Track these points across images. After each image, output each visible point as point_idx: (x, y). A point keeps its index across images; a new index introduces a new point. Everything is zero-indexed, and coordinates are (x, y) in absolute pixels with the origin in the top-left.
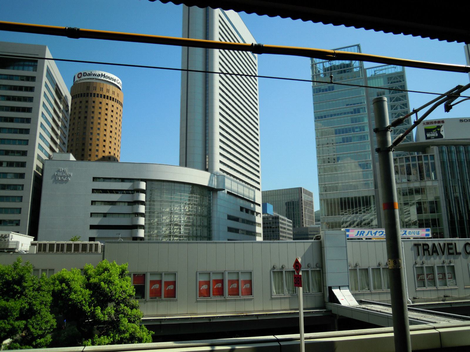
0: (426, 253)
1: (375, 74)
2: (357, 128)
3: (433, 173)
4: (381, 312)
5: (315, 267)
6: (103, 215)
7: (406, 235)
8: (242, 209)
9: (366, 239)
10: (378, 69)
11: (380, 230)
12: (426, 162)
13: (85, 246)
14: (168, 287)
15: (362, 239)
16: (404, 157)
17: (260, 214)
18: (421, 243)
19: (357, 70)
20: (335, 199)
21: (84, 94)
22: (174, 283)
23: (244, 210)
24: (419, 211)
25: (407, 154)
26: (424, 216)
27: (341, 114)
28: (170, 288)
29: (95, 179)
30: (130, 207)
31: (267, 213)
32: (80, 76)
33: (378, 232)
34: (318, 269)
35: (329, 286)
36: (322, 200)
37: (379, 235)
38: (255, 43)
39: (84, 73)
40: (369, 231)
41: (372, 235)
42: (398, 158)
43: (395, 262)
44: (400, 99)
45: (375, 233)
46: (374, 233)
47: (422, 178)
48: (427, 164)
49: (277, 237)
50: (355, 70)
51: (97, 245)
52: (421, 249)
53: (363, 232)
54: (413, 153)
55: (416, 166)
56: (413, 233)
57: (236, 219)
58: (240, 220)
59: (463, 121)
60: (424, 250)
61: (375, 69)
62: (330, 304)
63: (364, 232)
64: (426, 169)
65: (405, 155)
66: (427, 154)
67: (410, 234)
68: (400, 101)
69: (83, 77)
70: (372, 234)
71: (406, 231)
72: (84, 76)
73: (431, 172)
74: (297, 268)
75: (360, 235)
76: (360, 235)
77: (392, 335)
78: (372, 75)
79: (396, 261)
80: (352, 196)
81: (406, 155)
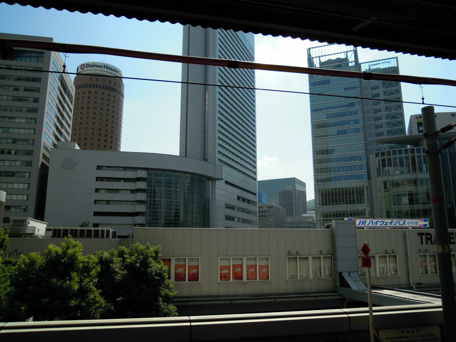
0: (429, 241)
1: (370, 68)
2: (351, 121)
3: (425, 165)
4: (391, 296)
5: (327, 253)
6: (106, 202)
7: (405, 225)
8: (239, 198)
9: (412, 228)
10: (372, 63)
11: (381, 220)
12: (419, 154)
13: (89, 232)
14: (178, 270)
15: (364, 228)
16: (397, 149)
17: (256, 203)
18: (424, 232)
19: (353, 65)
20: (336, 188)
21: (87, 85)
22: (197, 267)
23: (241, 199)
24: (411, 202)
25: (399, 146)
26: (416, 207)
27: (336, 107)
28: (193, 272)
29: (99, 168)
30: (133, 195)
31: (262, 202)
32: (83, 67)
33: (379, 222)
34: (329, 256)
35: (340, 271)
36: (317, 190)
37: (380, 225)
38: (240, 33)
39: (87, 65)
40: (397, 221)
41: (373, 225)
42: (391, 150)
43: (443, 247)
44: (394, 93)
45: (376, 223)
46: (375, 223)
47: (414, 170)
48: (419, 157)
49: (4, 222)
50: (350, 64)
51: (108, 231)
52: (424, 237)
53: (364, 222)
54: (406, 145)
55: (409, 159)
56: (412, 223)
57: (233, 208)
58: (236, 208)
59: (455, 115)
60: (427, 239)
61: (370, 64)
62: (341, 288)
63: (366, 222)
64: (418, 162)
65: (398, 148)
66: (420, 146)
67: (409, 224)
68: (394, 95)
69: (86, 69)
70: (374, 224)
71: (405, 222)
72: (87, 67)
73: (423, 165)
74: (366, 251)
75: (362, 224)
76: (362, 224)
77: (441, 309)
78: (366, 70)
79: (444, 247)
80: (349, 187)
81: (399, 147)
